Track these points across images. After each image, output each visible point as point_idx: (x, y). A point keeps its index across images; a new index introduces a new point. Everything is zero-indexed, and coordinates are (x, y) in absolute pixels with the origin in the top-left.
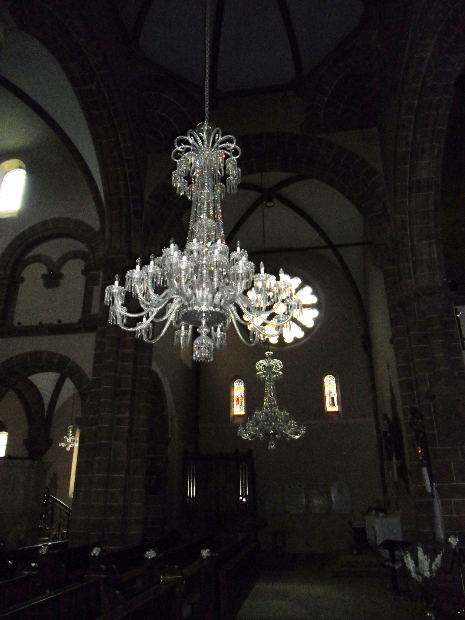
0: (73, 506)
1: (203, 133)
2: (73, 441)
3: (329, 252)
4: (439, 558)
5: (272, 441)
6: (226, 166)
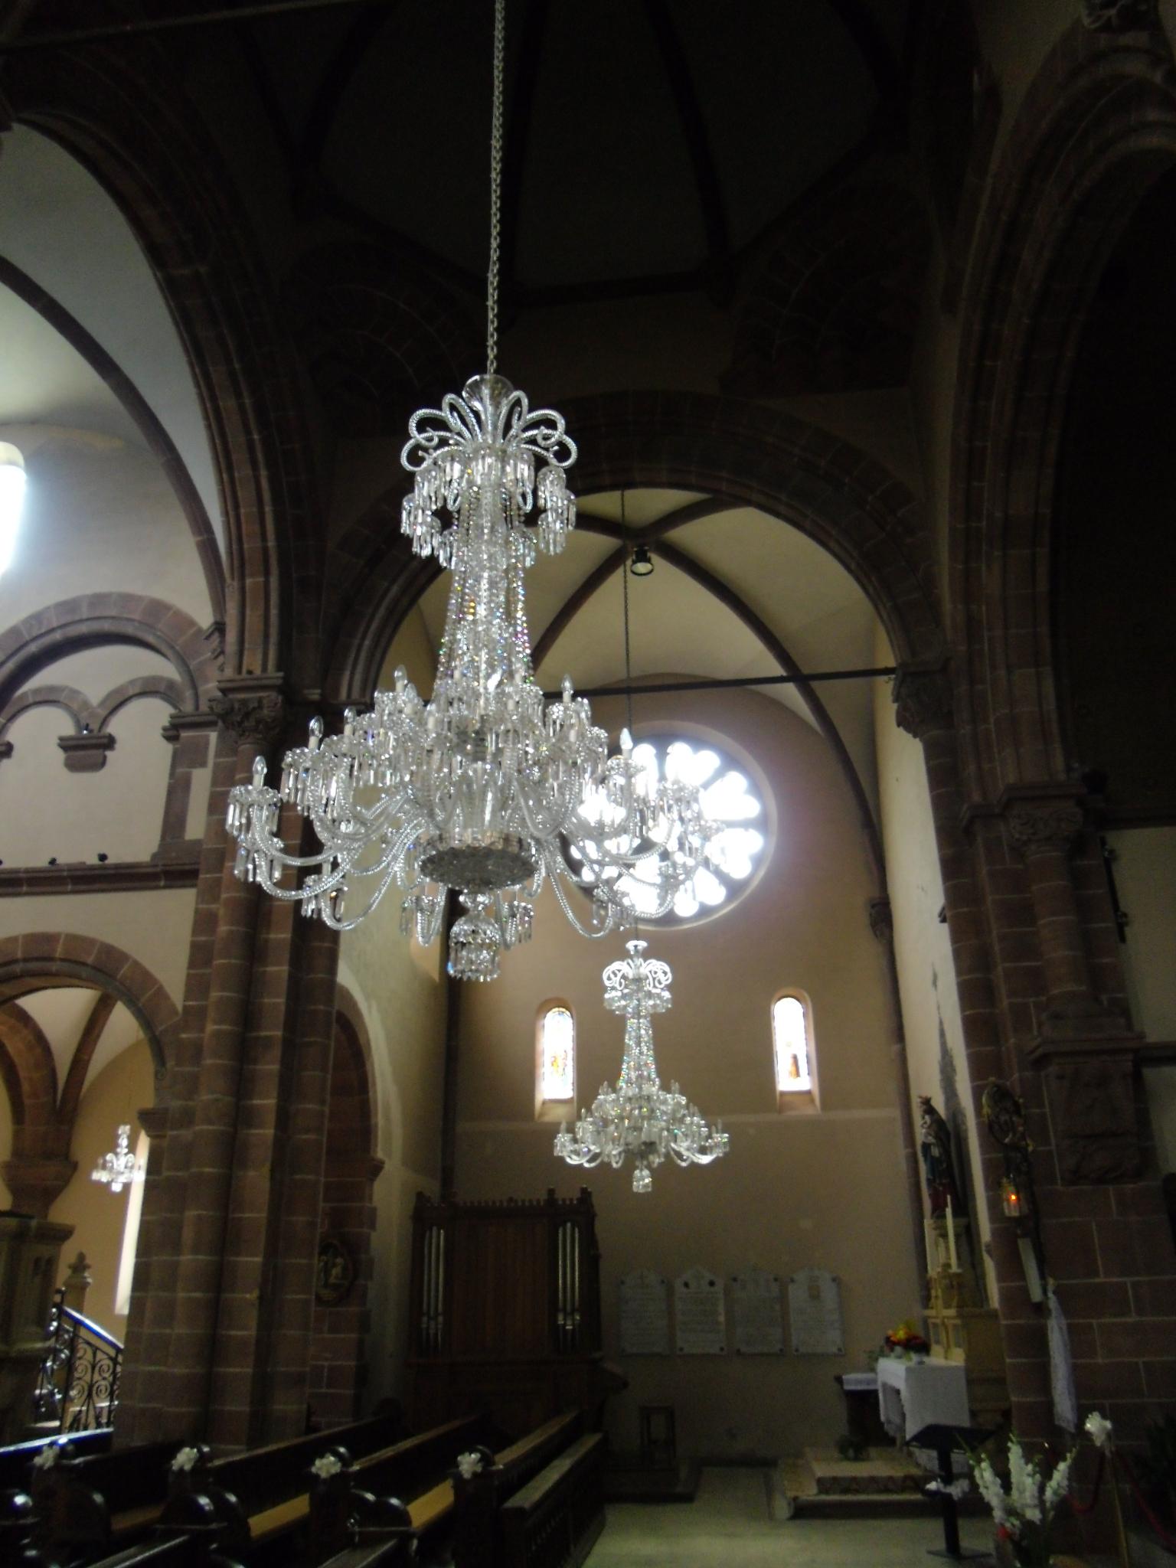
0: (130, 1338)
1: (481, 400)
2: (130, 1168)
3: (790, 693)
4: (1062, 1471)
5: (641, 1170)
6: (539, 486)
